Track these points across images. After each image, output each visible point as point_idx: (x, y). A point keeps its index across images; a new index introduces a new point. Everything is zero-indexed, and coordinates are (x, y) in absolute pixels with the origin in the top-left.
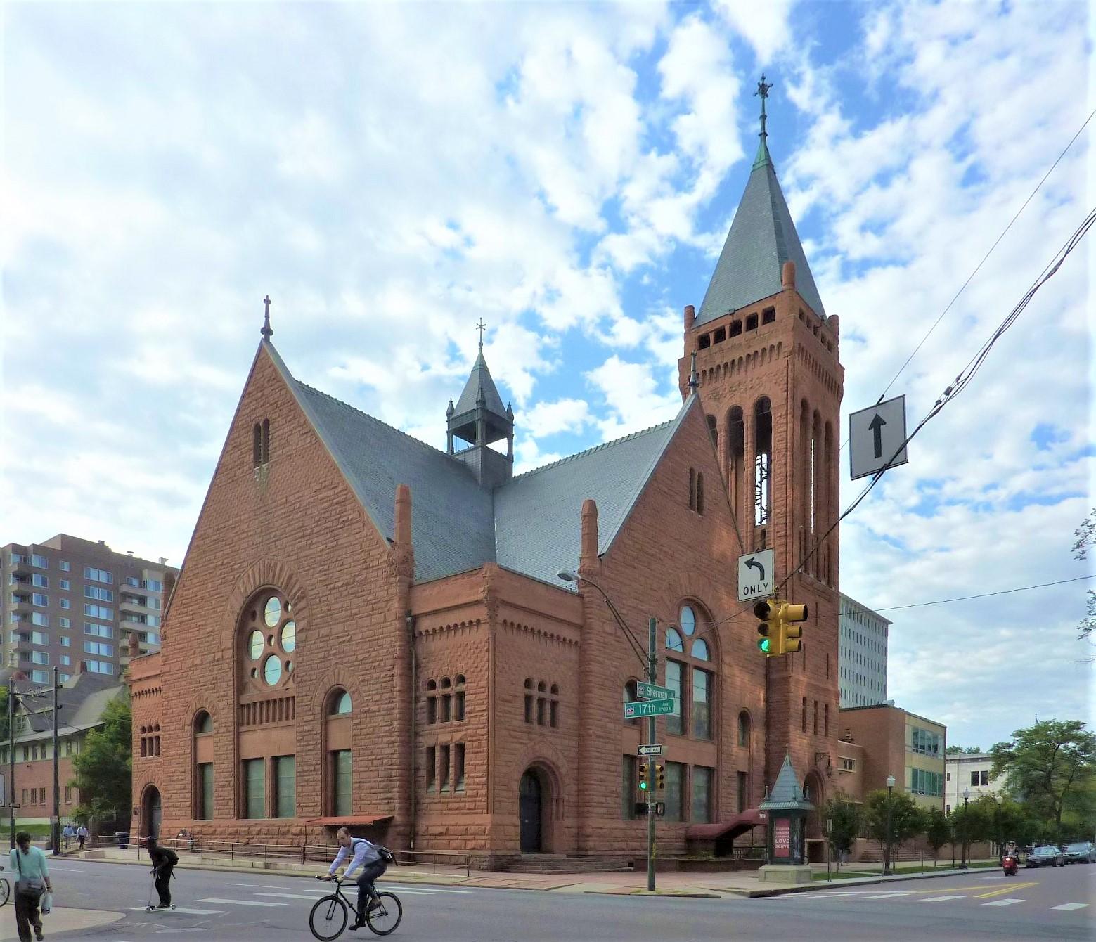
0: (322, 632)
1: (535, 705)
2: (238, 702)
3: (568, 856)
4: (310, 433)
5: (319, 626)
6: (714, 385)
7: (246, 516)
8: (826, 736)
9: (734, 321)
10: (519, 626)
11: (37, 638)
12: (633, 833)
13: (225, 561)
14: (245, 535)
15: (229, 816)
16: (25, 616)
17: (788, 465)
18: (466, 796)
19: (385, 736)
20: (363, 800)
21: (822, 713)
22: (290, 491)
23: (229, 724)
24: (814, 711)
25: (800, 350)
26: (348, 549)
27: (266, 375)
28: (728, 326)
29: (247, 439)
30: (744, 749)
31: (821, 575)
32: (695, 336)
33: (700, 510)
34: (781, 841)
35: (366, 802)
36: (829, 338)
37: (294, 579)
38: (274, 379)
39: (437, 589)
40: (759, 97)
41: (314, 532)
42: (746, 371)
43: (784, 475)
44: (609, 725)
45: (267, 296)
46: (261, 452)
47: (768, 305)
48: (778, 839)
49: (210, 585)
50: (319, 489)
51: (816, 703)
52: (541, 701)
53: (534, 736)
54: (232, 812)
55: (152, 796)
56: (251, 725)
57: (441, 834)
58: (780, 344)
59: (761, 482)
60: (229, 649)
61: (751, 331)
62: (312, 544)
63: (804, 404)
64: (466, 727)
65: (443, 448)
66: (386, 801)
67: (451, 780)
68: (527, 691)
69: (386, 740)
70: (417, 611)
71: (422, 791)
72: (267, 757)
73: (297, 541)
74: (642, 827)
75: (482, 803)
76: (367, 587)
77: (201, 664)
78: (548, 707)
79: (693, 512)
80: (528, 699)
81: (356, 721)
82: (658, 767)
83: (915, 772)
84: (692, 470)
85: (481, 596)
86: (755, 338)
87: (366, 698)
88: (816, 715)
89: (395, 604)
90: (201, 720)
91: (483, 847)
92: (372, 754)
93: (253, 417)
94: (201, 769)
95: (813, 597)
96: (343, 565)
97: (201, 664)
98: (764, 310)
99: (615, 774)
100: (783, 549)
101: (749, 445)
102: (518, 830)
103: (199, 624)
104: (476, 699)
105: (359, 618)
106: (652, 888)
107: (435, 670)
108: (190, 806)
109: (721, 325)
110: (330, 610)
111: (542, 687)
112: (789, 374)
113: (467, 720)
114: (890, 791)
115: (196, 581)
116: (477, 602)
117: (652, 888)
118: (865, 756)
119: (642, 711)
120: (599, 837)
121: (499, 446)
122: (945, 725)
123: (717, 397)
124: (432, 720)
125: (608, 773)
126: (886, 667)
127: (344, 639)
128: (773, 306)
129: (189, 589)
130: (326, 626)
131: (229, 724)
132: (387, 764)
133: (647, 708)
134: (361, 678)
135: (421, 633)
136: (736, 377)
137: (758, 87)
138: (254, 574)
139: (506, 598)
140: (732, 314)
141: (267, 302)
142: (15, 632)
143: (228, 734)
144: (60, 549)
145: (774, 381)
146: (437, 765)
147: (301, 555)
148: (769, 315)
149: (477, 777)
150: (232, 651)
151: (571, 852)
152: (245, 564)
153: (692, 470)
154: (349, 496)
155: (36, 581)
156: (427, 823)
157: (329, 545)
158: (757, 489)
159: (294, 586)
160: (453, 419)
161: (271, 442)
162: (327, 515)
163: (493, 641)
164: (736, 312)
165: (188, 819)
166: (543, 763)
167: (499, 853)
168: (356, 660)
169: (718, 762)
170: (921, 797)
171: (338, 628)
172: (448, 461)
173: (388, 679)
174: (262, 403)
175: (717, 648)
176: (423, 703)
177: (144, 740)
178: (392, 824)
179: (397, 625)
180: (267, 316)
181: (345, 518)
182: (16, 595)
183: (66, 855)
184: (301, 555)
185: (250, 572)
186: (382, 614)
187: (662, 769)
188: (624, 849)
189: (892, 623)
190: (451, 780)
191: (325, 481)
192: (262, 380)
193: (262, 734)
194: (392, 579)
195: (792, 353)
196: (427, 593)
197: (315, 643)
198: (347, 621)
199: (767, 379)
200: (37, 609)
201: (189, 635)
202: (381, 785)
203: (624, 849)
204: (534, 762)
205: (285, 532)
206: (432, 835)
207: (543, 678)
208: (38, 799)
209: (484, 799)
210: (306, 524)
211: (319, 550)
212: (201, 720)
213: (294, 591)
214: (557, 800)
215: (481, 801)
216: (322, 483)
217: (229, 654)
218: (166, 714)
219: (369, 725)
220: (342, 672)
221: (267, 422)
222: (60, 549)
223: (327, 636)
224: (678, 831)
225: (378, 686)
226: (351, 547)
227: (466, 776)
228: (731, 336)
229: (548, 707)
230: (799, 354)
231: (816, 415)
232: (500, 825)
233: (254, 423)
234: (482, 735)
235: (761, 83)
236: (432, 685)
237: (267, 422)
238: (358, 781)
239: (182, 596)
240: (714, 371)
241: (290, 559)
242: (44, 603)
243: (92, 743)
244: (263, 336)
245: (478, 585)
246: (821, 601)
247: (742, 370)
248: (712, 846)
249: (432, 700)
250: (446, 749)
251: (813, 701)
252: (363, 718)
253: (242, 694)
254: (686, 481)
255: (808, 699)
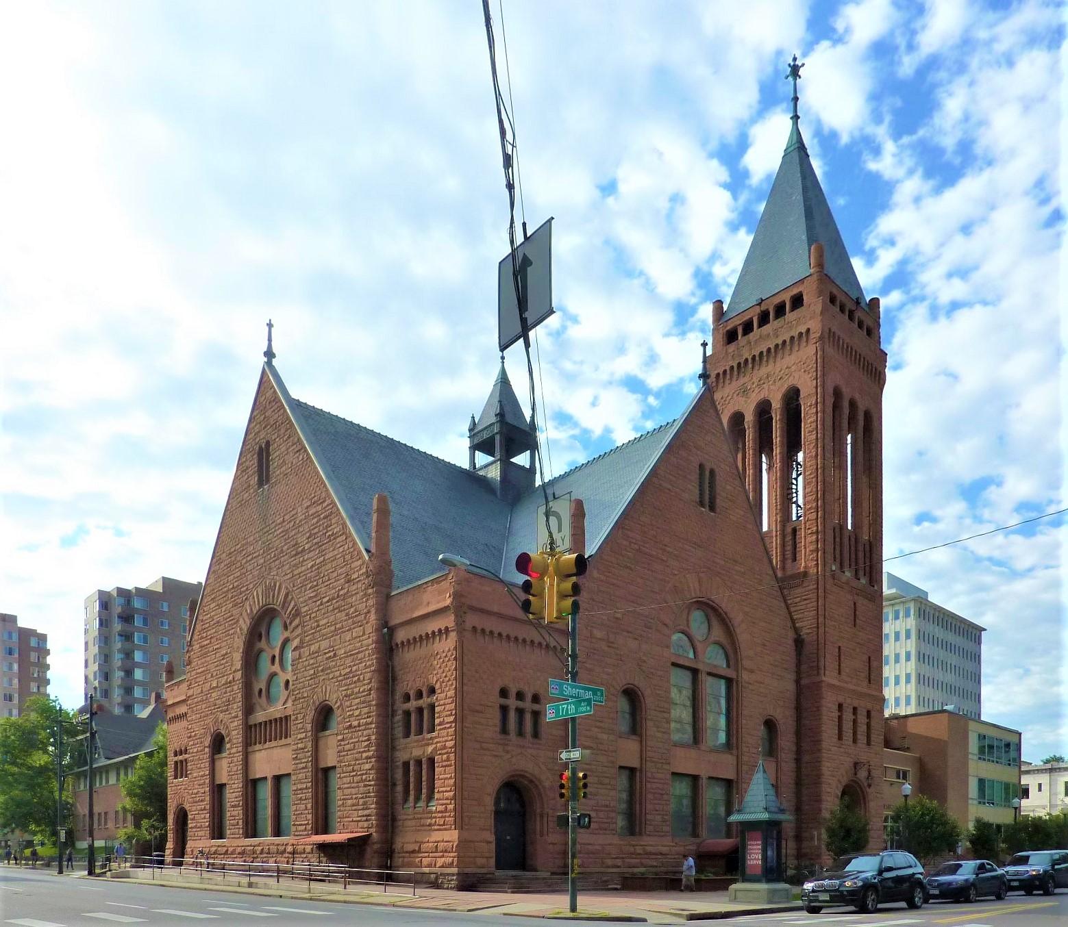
0: (313, 648)
1: (512, 716)
2: (247, 723)
3: (553, 873)
4: (303, 451)
5: (310, 643)
6: (742, 380)
7: (252, 538)
8: (869, 743)
9: (762, 311)
10: (508, 637)
11: (138, 674)
12: (632, 849)
13: (236, 584)
14: (251, 557)
15: (238, 836)
16: (128, 655)
17: (819, 457)
18: (436, 812)
19: (364, 751)
20: (346, 817)
21: (862, 719)
22: (287, 510)
23: (239, 745)
24: (867, 720)
25: (829, 337)
26: (333, 563)
27: (270, 399)
28: (757, 317)
29: (252, 462)
30: (772, 759)
31: (861, 573)
32: (722, 331)
33: (712, 508)
34: (753, 856)
35: (349, 819)
36: (868, 322)
37: (290, 597)
38: (274, 400)
39: (410, 598)
40: (790, 79)
41: (306, 548)
42: (775, 362)
43: (815, 467)
44: (600, 736)
45: (270, 320)
46: (264, 475)
47: (795, 291)
48: (751, 854)
49: (223, 609)
50: (310, 506)
51: (855, 709)
52: (521, 712)
53: (509, 748)
54: (241, 832)
55: (182, 817)
56: (257, 745)
57: (413, 852)
58: (808, 330)
59: (796, 479)
60: (239, 670)
61: (779, 319)
62: (304, 561)
63: (837, 393)
64: (436, 740)
65: (465, 464)
66: (365, 818)
67: (412, 798)
68: (503, 701)
69: (364, 755)
70: (395, 621)
71: (399, 807)
72: (270, 776)
73: (292, 559)
74: (642, 843)
75: (450, 819)
76: (349, 600)
77: (217, 687)
78: (528, 717)
79: (703, 509)
80: (504, 709)
81: (340, 737)
82: (581, 775)
83: (981, 782)
84: (701, 466)
85: (448, 602)
86: (782, 327)
87: (348, 714)
88: (855, 721)
89: (373, 616)
90: (218, 743)
91: (451, 865)
92: (353, 771)
93: (257, 441)
94: (218, 790)
95: (849, 597)
96: (329, 580)
97: (217, 687)
98: (792, 297)
99: (609, 787)
100: (813, 547)
101: (778, 439)
102: (493, 846)
103: (215, 647)
104: (445, 705)
105: (343, 632)
106: (573, 908)
107: (409, 682)
108: (209, 826)
109: (749, 317)
110: (318, 626)
111: (520, 696)
112: (819, 361)
113: (436, 732)
114: (906, 800)
115: (212, 606)
116: (446, 609)
117: (573, 908)
118: (922, 766)
119: (562, 713)
120: (588, 853)
121: (522, 459)
122: (1020, 731)
123: (745, 392)
124: (407, 735)
125: (600, 786)
126: (980, 676)
127: (330, 654)
128: (801, 292)
129: (207, 614)
130: (316, 642)
131: (239, 745)
132: (365, 780)
133: (567, 709)
134: (344, 693)
135: (397, 645)
136: (764, 371)
137: (790, 69)
138: (257, 594)
139: (475, 603)
140: (759, 304)
141: (270, 325)
142: (119, 669)
143: (238, 755)
144: (161, 591)
145: (803, 370)
146: (412, 780)
147: (295, 573)
148: (797, 301)
149: (446, 791)
150: (241, 672)
151: (555, 870)
152: (251, 586)
153: (701, 466)
154: (334, 510)
155: (138, 621)
156: (403, 841)
157: (318, 561)
158: (794, 487)
159: (289, 605)
160: (474, 435)
161: (271, 463)
162: (316, 530)
163: (461, 646)
164: (763, 303)
165: (207, 839)
166: (523, 776)
167: (467, 870)
168: (340, 675)
169: (738, 774)
170: (988, 808)
171: (325, 644)
172: (471, 477)
173: (366, 693)
174: (264, 425)
175: (736, 652)
176: (399, 717)
177: (176, 762)
178: (370, 842)
179: (374, 637)
180: (270, 340)
181: (330, 533)
182: (121, 635)
183: (99, 875)
184: (295, 573)
185: (255, 594)
186: (362, 628)
187: (585, 776)
188: (619, 867)
189: (986, 630)
190: (412, 798)
191: (315, 496)
192: (264, 402)
193: (266, 753)
194: (370, 591)
195: (821, 338)
196: (403, 602)
197: (306, 660)
198: (332, 636)
199: (798, 370)
200: (139, 648)
201: (208, 659)
202: (361, 801)
203: (619, 867)
204: (513, 776)
205: (282, 551)
206: (407, 852)
207: (522, 687)
208: (103, 823)
209: (452, 814)
210: (299, 542)
211: (309, 567)
212: (218, 743)
213: (289, 610)
214: (542, 816)
215: (450, 816)
216: (311, 499)
217: (239, 675)
218: (190, 737)
219: (351, 741)
220: (328, 688)
221: (268, 444)
222: (161, 591)
223: (316, 652)
224: (687, 848)
225: (357, 701)
226: (335, 562)
227: (436, 790)
228: (760, 326)
229: (528, 717)
230: (829, 340)
231: (853, 404)
232: (471, 841)
233: (258, 446)
234: (451, 748)
235: (792, 64)
236: (407, 698)
237: (268, 444)
238: (342, 798)
239: (202, 621)
240: (742, 365)
241: (286, 577)
242: (145, 641)
243: (142, 768)
244: (266, 359)
245: (445, 592)
246: (861, 601)
247: (771, 361)
248: (722, 863)
249: (407, 714)
250: (419, 763)
251: (852, 707)
252: (346, 733)
253: (251, 714)
254: (695, 477)
255: (844, 705)
